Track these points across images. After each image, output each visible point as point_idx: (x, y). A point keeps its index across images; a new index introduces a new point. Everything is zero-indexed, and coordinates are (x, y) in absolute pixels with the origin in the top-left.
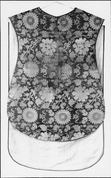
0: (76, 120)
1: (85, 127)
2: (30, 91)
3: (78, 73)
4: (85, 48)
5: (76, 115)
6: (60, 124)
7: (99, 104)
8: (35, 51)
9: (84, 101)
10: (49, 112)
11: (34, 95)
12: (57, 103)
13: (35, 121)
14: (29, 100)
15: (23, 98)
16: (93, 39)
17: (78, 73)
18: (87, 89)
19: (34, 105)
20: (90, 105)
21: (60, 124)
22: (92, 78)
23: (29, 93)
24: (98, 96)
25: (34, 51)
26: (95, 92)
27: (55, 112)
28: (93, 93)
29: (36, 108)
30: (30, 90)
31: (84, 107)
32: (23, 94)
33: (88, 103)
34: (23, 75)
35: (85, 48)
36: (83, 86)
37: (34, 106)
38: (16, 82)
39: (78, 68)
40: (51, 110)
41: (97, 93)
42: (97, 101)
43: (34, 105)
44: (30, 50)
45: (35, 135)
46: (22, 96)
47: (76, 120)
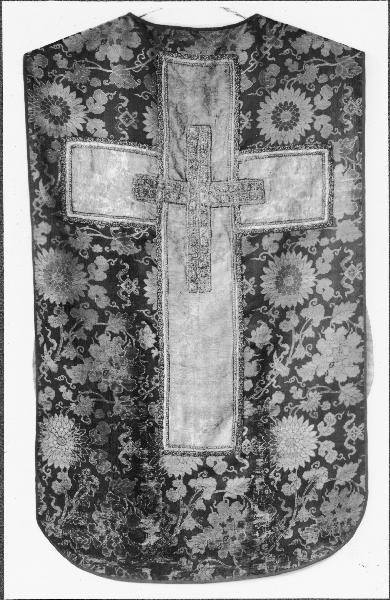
0: (349, 258)
1: (323, 239)
2: (291, 366)
3: (350, 427)
4: (334, 512)
5: (352, 279)
6: (297, 253)
7: (51, 319)
8: (49, 505)
9: (329, 332)
10: (333, 290)
11: (278, 355)
12: (310, 329)
13: (270, 263)
14: (62, 330)
15: (85, 338)
16: (310, 544)
17: (350, 427)
18: (320, 374)
19: (278, 322)
20: (311, 320)
21: (297, 253)
22: (306, 415)
23: (63, 358)
24: (288, 355)
25: (52, 504)
26: (65, 367)
27: (315, 295)
28: (299, 363)
29: (270, 313)
30: (293, 373)
31: (329, 311)
32: (315, 351)
33: (316, 324)
34: (89, 422)
35: (223, 525)
36: (335, 385)
37: (275, 316)
38: (339, 389)
39: (350, 442)
40: (326, 298)
41: (57, 363)
42: (56, 333)
43: (278, 322)
44: (66, 508)
45: (38, 205)
46: (319, 342)
47: (349, 258)
